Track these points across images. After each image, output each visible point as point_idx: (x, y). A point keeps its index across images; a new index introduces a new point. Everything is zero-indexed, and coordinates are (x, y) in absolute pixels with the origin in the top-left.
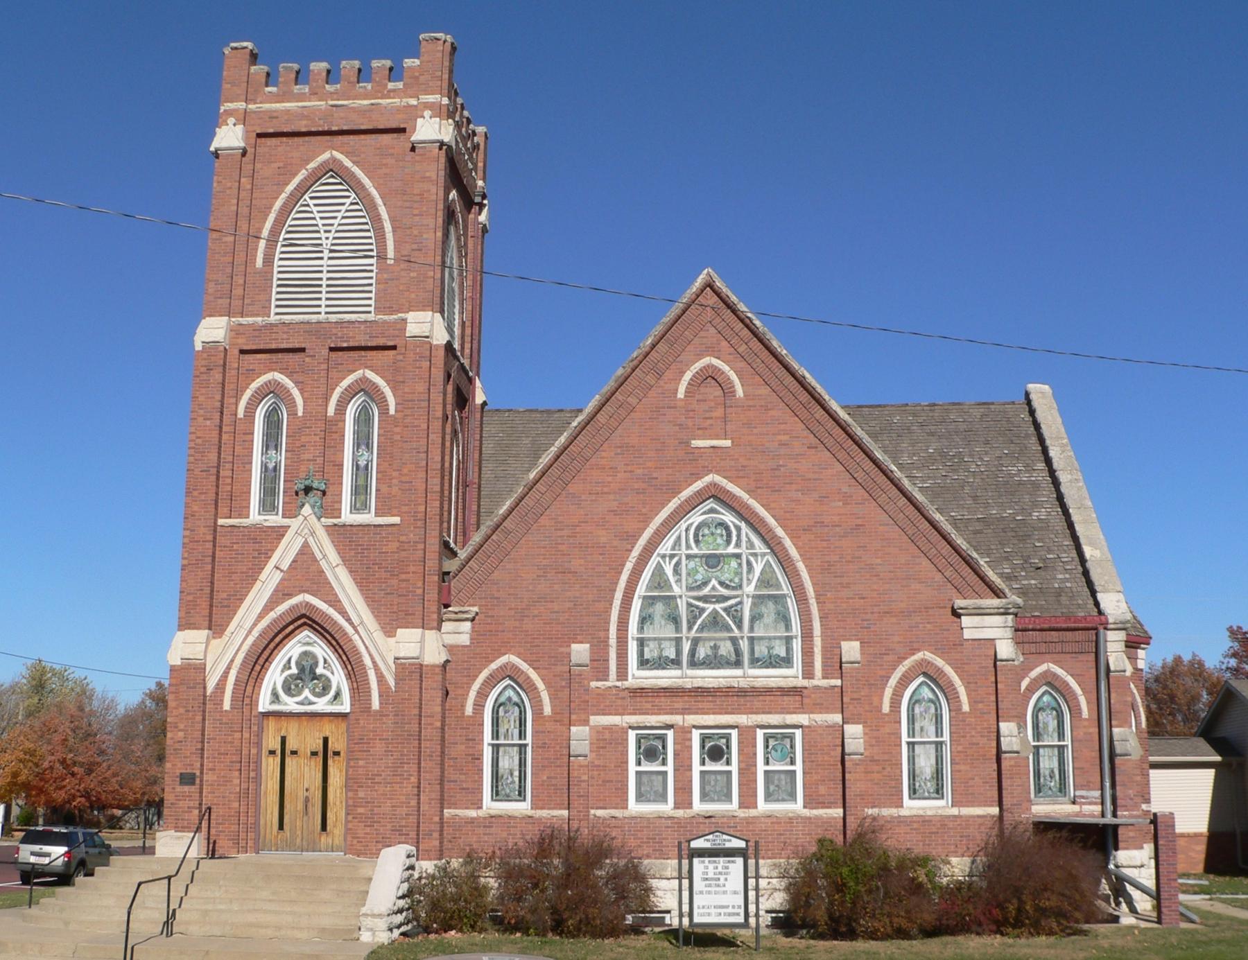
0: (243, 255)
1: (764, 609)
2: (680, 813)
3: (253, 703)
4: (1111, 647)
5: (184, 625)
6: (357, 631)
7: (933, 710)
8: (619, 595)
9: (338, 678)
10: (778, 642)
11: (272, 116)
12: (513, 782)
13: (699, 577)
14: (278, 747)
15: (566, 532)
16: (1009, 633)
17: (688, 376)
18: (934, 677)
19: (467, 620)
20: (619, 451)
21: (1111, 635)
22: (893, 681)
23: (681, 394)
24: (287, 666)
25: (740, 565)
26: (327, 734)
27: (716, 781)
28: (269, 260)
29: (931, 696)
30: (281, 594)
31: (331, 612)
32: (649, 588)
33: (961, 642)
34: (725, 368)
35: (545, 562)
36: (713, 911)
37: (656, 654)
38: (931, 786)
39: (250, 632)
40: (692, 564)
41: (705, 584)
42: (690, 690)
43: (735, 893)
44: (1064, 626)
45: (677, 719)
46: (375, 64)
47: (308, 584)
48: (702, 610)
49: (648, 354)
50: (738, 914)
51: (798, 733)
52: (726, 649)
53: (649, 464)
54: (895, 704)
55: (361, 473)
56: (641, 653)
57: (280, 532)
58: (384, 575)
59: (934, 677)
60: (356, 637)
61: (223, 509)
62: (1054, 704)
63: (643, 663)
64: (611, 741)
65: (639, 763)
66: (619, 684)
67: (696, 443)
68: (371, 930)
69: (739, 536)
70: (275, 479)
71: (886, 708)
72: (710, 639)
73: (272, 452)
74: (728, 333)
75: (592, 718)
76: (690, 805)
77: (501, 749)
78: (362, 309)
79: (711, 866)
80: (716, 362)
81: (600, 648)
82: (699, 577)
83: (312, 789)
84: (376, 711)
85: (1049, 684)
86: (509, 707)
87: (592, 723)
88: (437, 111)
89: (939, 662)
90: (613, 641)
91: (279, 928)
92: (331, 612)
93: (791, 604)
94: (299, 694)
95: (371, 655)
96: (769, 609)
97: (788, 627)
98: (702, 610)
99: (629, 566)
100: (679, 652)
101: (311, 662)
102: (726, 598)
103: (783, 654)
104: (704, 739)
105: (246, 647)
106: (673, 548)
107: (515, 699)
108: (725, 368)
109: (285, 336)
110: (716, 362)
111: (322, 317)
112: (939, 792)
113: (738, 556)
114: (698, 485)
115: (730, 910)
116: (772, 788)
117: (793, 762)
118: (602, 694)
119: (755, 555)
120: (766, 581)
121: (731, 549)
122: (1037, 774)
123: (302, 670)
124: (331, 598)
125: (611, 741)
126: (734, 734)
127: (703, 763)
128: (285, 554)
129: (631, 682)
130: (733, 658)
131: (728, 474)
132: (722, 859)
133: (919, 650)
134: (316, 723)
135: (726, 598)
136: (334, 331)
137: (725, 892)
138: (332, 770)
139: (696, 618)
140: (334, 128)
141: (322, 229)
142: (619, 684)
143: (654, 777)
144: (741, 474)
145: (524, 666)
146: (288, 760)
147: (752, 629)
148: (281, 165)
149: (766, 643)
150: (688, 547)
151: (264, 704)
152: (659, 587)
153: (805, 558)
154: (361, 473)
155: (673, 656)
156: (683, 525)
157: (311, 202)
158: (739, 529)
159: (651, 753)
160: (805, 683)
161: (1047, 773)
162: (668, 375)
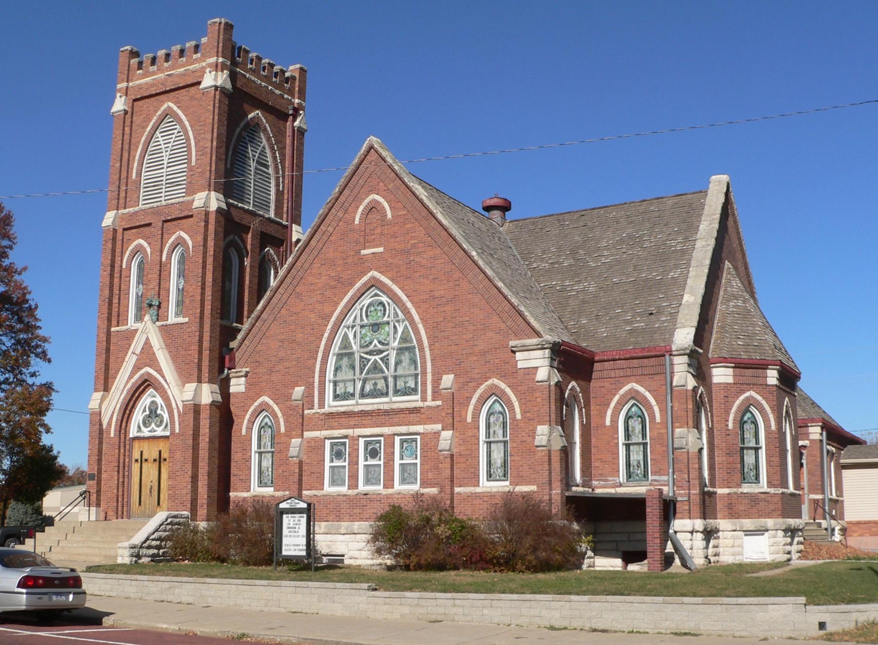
0: (125, 173)
1: (403, 357)
3: (126, 433)
4: (677, 368)
5: (96, 390)
7: (501, 419)
8: (320, 355)
10: (410, 378)
11: (140, 87)
13: (367, 339)
16: (547, 362)
19: (242, 376)
21: (677, 360)
24: (144, 411)
26: (161, 448)
28: (139, 174)
29: (501, 409)
30: (137, 368)
32: (340, 348)
33: (516, 371)
36: (292, 548)
37: (343, 391)
38: (500, 472)
40: (364, 331)
41: (371, 343)
44: (640, 355)
45: (349, 432)
46: (188, 45)
48: (369, 360)
49: (337, 199)
52: (381, 384)
53: (339, 269)
54: (614, 420)
56: (335, 391)
60: (169, 391)
61: (114, 322)
62: (640, 413)
63: (336, 397)
64: (317, 447)
65: (332, 461)
67: (363, 252)
71: (469, 419)
76: (357, 487)
78: (178, 196)
81: (310, 387)
82: (367, 339)
88: (216, 67)
89: (503, 385)
90: (316, 384)
103: (413, 386)
104: (367, 444)
105: (121, 400)
107: (269, 424)
111: (164, 203)
113: (388, 323)
114: (365, 279)
116: (406, 475)
118: (311, 418)
119: (398, 321)
120: (405, 339)
121: (385, 319)
123: (151, 412)
127: (366, 460)
129: (327, 409)
131: (382, 270)
132: (297, 515)
133: (490, 378)
134: (155, 442)
135: (382, 352)
137: (298, 536)
138: (163, 470)
139: (365, 366)
140: (168, 89)
142: (319, 411)
146: (144, 464)
147: (396, 370)
149: (403, 379)
150: (362, 320)
152: (345, 348)
156: (358, 306)
158: (389, 304)
159: (373, 453)
161: (635, 463)
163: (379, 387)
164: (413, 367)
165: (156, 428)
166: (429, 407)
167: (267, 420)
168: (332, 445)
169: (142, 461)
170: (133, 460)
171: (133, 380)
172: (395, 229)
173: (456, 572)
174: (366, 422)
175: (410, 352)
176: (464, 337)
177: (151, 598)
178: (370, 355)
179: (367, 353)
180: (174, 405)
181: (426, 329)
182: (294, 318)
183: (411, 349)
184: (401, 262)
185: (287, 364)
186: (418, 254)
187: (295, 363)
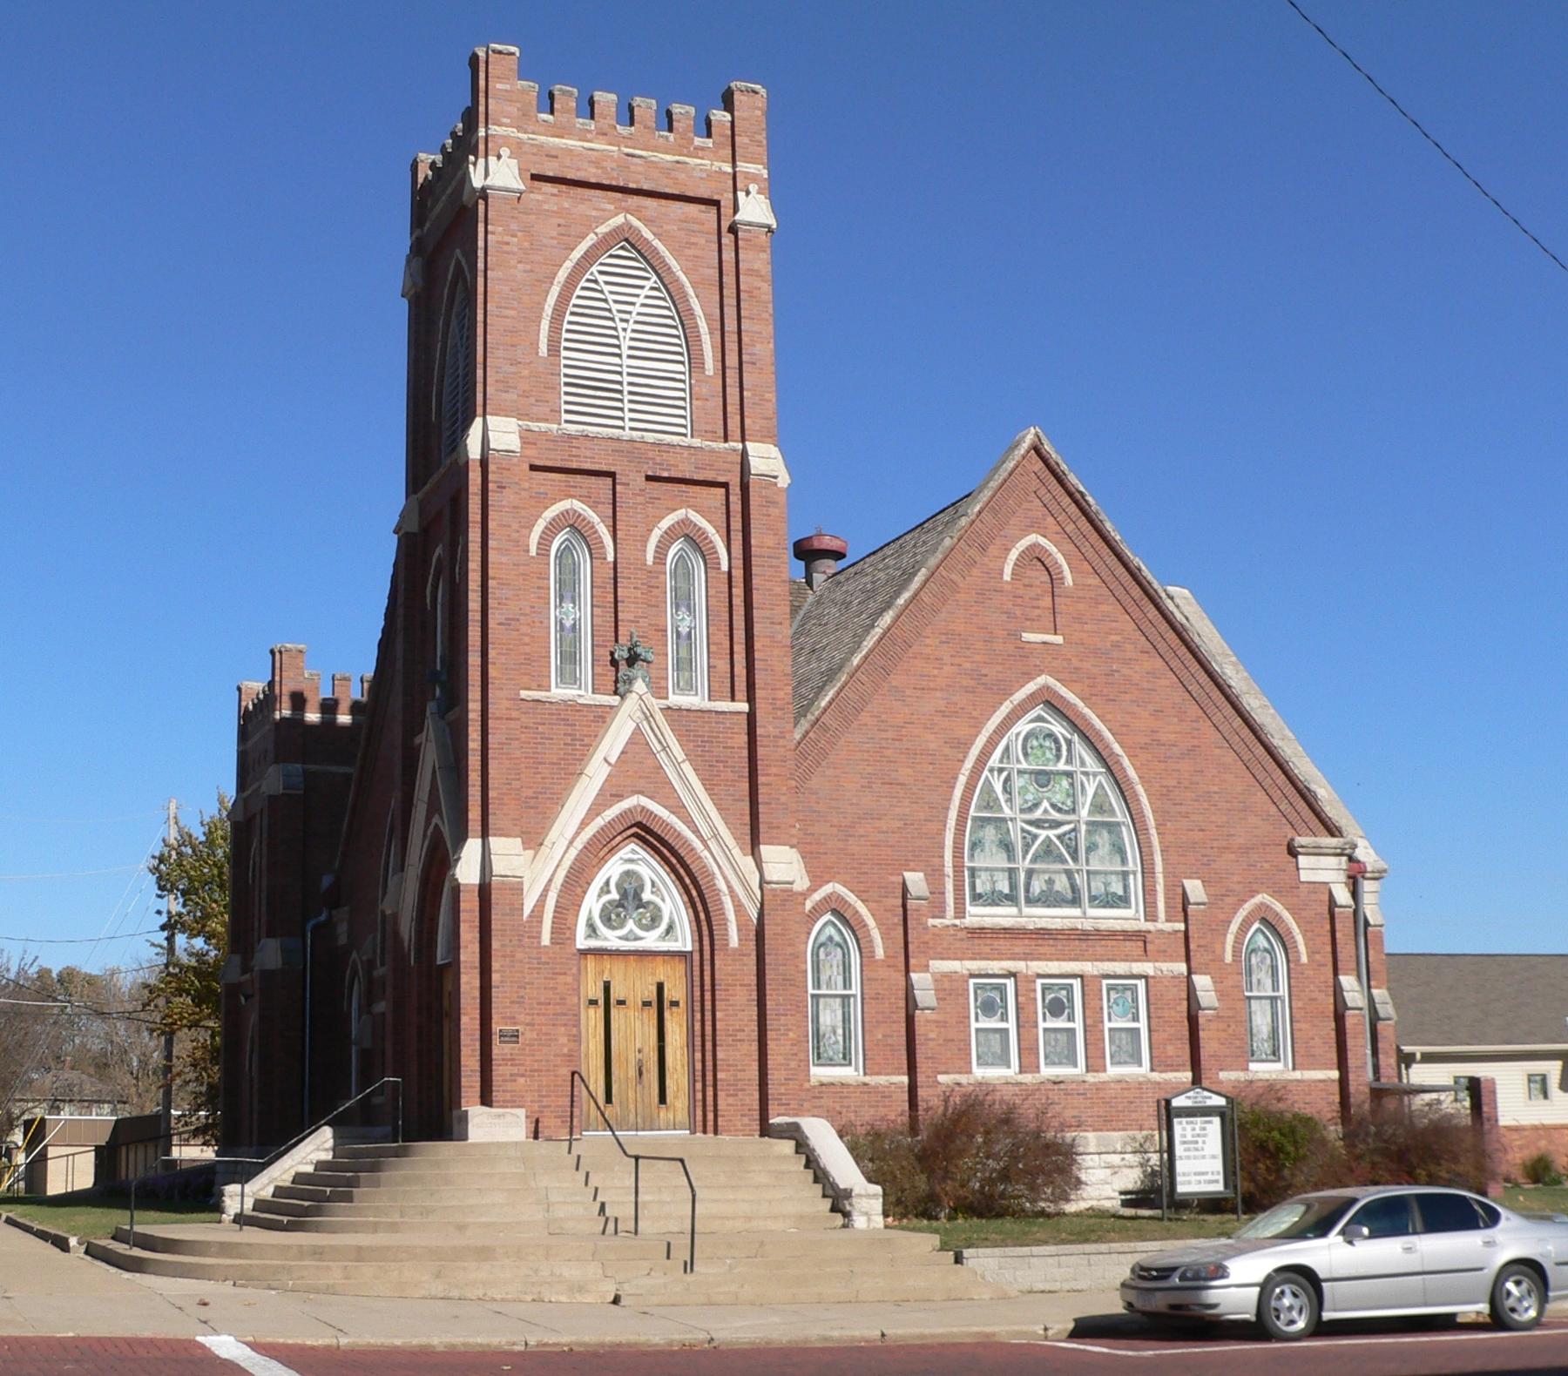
1: (1097, 838)
2: (1027, 1078)
6: (707, 847)
9: (673, 905)
10: (1114, 877)
12: (837, 1042)
13: (1030, 797)
14: (653, 997)
15: (890, 734)
17: (1014, 555)
18: (1271, 924)
20: (943, 638)
22: (1234, 927)
23: (1007, 577)
24: (605, 889)
25: (1072, 785)
26: (662, 978)
27: (1056, 1040)
28: (554, 349)
29: (1266, 945)
30: (608, 794)
34: (1053, 549)
35: (870, 769)
37: (988, 887)
38: (1267, 1047)
39: (571, 843)
41: (1036, 805)
42: (1032, 932)
43: (1214, 1157)
47: (642, 782)
48: (1035, 837)
51: (1141, 984)
52: (1061, 884)
53: (978, 658)
55: (684, 643)
57: (602, 716)
58: (731, 776)
59: (1271, 924)
66: (957, 922)
67: (1027, 636)
68: (866, 1214)
69: (1069, 750)
70: (576, 641)
72: (1044, 872)
73: (568, 606)
74: (1054, 508)
77: (822, 1001)
79: (1189, 1127)
80: (1042, 541)
81: (935, 876)
83: (646, 1050)
84: (735, 950)
85: (835, 912)
86: (831, 948)
89: (1278, 907)
90: (949, 870)
91: (749, 1219)
93: (1128, 837)
94: (622, 926)
95: (725, 878)
96: (1103, 839)
97: (1124, 861)
98: (1035, 837)
99: (962, 780)
100: (1013, 886)
101: (635, 885)
102: (1058, 824)
105: (567, 863)
106: (1001, 761)
107: (837, 938)
108: (1053, 549)
110: (1042, 541)
111: (627, 434)
112: (846, 1059)
113: (1069, 775)
115: (1209, 1177)
117: (1136, 1018)
118: (938, 934)
119: (1086, 774)
120: (1099, 806)
122: (818, 1035)
123: (624, 894)
124: (671, 802)
125: (951, 988)
126: (1077, 983)
128: (613, 742)
129: (968, 921)
130: (1069, 896)
132: (1199, 1119)
133: (1258, 892)
134: (648, 963)
135: (1058, 824)
136: (651, 454)
137: (1204, 1157)
140: (632, 185)
141: (618, 316)
142: (957, 922)
143: (991, 1036)
144: (1074, 677)
145: (851, 898)
146: (614, 1012)
149: (1101, 878)
151: (582, 942)
152: (988, 807)
154: (684, 643)
155: (1006, 891)
156: (1014, 730)
157: (601, 278)
158: (1069, 743)
160: (1150, 926)
162: (993, 550)
163: (1057, 887)
166: (1161, 932)
167: (830, 931)
168: (1045, 989)
170: (682, 1004)
171: (599, 822)
172: (1081, 606)
173: (1218, 1217)
175: (997, 828)
176: (1213, 818)
178: (1038, 827)
179: (1030, 823)
181: (1149, 795)
183: (1113, 828)
184: (1095, 671)
186: (1127, 662)
187: (900, 824)
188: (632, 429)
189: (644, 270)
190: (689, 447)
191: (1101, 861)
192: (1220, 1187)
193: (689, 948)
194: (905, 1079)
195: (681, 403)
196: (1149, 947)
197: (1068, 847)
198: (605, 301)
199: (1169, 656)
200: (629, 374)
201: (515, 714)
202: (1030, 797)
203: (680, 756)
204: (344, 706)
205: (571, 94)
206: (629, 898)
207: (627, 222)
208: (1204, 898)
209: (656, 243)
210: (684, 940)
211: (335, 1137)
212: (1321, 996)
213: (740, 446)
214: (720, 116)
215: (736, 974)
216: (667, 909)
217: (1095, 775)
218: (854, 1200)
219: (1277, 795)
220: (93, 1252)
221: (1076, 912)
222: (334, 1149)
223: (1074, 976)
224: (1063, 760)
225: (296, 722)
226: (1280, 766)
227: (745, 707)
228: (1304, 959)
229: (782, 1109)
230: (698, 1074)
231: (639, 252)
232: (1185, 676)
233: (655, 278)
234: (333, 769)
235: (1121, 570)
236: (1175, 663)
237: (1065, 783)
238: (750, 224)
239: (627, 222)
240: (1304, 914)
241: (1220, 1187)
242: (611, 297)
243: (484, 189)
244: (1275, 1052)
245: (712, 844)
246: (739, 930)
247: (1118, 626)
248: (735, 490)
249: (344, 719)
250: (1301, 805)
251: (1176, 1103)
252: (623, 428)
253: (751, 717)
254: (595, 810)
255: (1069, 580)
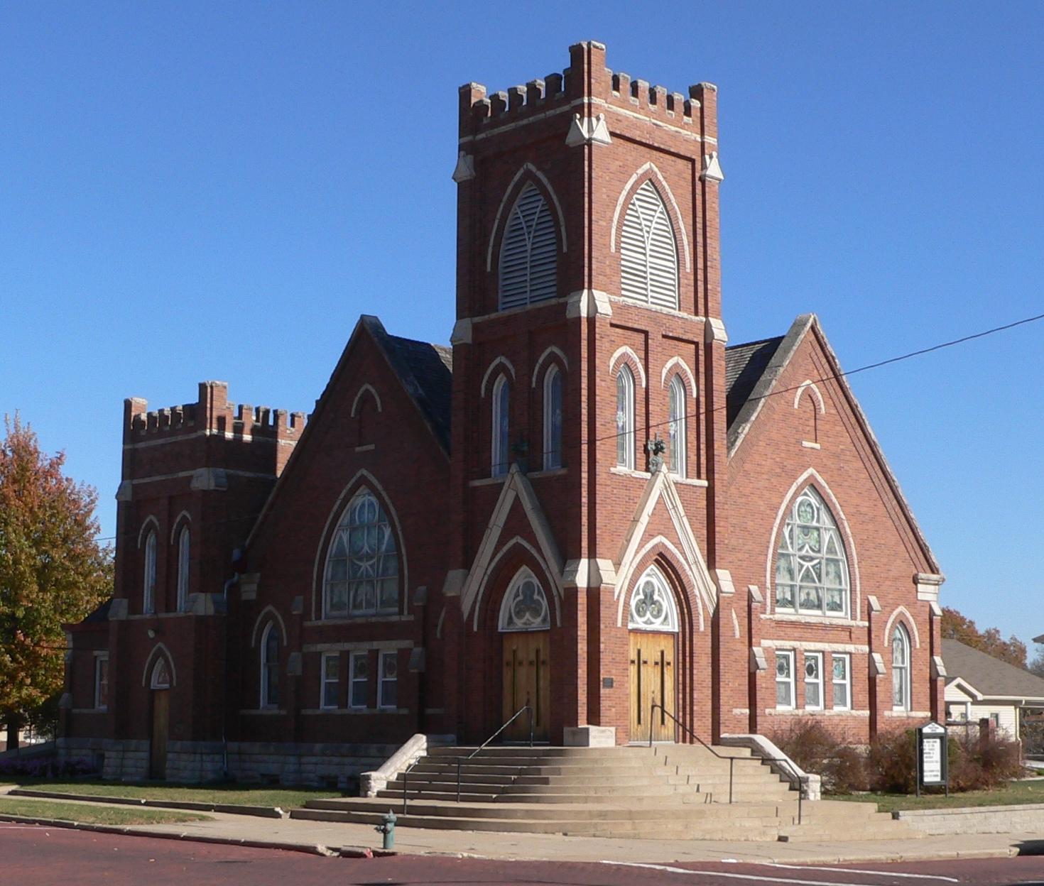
1: (830, 570)
7: (900, 646)
9: (668, 602)
14: (659, 660)
23: (796, 406)
24: (517, 595)
26: (663, 648)
29: (899, 636)
30: (648, 535)
31: (675, 551)
41: (803, 547)
43: (937, 762)
50: (937, 776)
51: (847, 657)
66: (771, 617)
72: (807, 587)
75: (763, 641)
84: (702, 632)
87: (304, 650)
92: (675, 551)
93: (843, 567)
94: (644, 615)
96: (832, 569)
97: (840, 583)
109: (636, 318)
113: (818, 529)
117: (844, 678)
120: (831, 550)
121: (815, 524)
124: (676, 541)
129: (777, 617)
130: (816, 603)
131: (820, 469)
135: (812, 559)
136: (665, 321)
137: (932, 762)
148: (621, 164)
153: (854, 536)
158: (818, 509)
160: (853, 623)
164: (838, 581)
165: (653, 620)
166: (858, 627)
169: (639, 663)
170: (672, 664)
174: (807, 635)
175: (835, 565)
177: (974, 830)
178: (804, 560)
180: (555, 593)
182: (744, 500)
183: (836, 562)
185: (740, 556)
187: (747, 555)
188: (652, 303)
189: (656, 200)
190: (682, 318)
191: (828, 582)
192: (938, 779)
193: (676, 630)
194: (747, 711)
195: (672, 288)
196: (853, 635)
197: (816, 573)
198: (638, 218)
199: (866, 460)
200: (651, 267)
201: (608, 482)
202: (800, 542)
203: (683, 513)
204: (247, 428)
205: (628, 79)
206: (649, 599)
207: (651, 168)
208: (879, 608)
209: (664, 183)
210: (674, 626)
211: (428, 741)
212: (924, 668)
213: (704, 319)
214: (695, 103)
215: (702, 645)
216: (665, 605)
217: (829, 530)
218: (810, 783)
219: (909, 546)
220: (294, 815)
221: (818, 612)
222: (427, 749)
223: (845, 653)
224: (815, 519)
225: (220, 438)
226: (912, 530)
227: (705, 483)
228: (918, 646)
229: (726, 729)
230: (681, 706)
231: (656, 188)
232: (873, 474)
233: (662, 206)
234: (241, 473)
235: (846, 406)
236: (868, 465)
237: (816, 534)
238: (712, 177)
239: (651, 168)
240: (918, 618)
241: (938, 779)
242: (642, 216)
243: (590, 139)
244: (901, 700)
245: (694, 567)
246: (704, 620)
247: (844, 440)
248: (701, 347)
249: (247, 437)
250: (920, 554)
251: (926, 730)
252: (647, 302)
253: (710, 492)
254: (641, 546)
255: (823, 411)
